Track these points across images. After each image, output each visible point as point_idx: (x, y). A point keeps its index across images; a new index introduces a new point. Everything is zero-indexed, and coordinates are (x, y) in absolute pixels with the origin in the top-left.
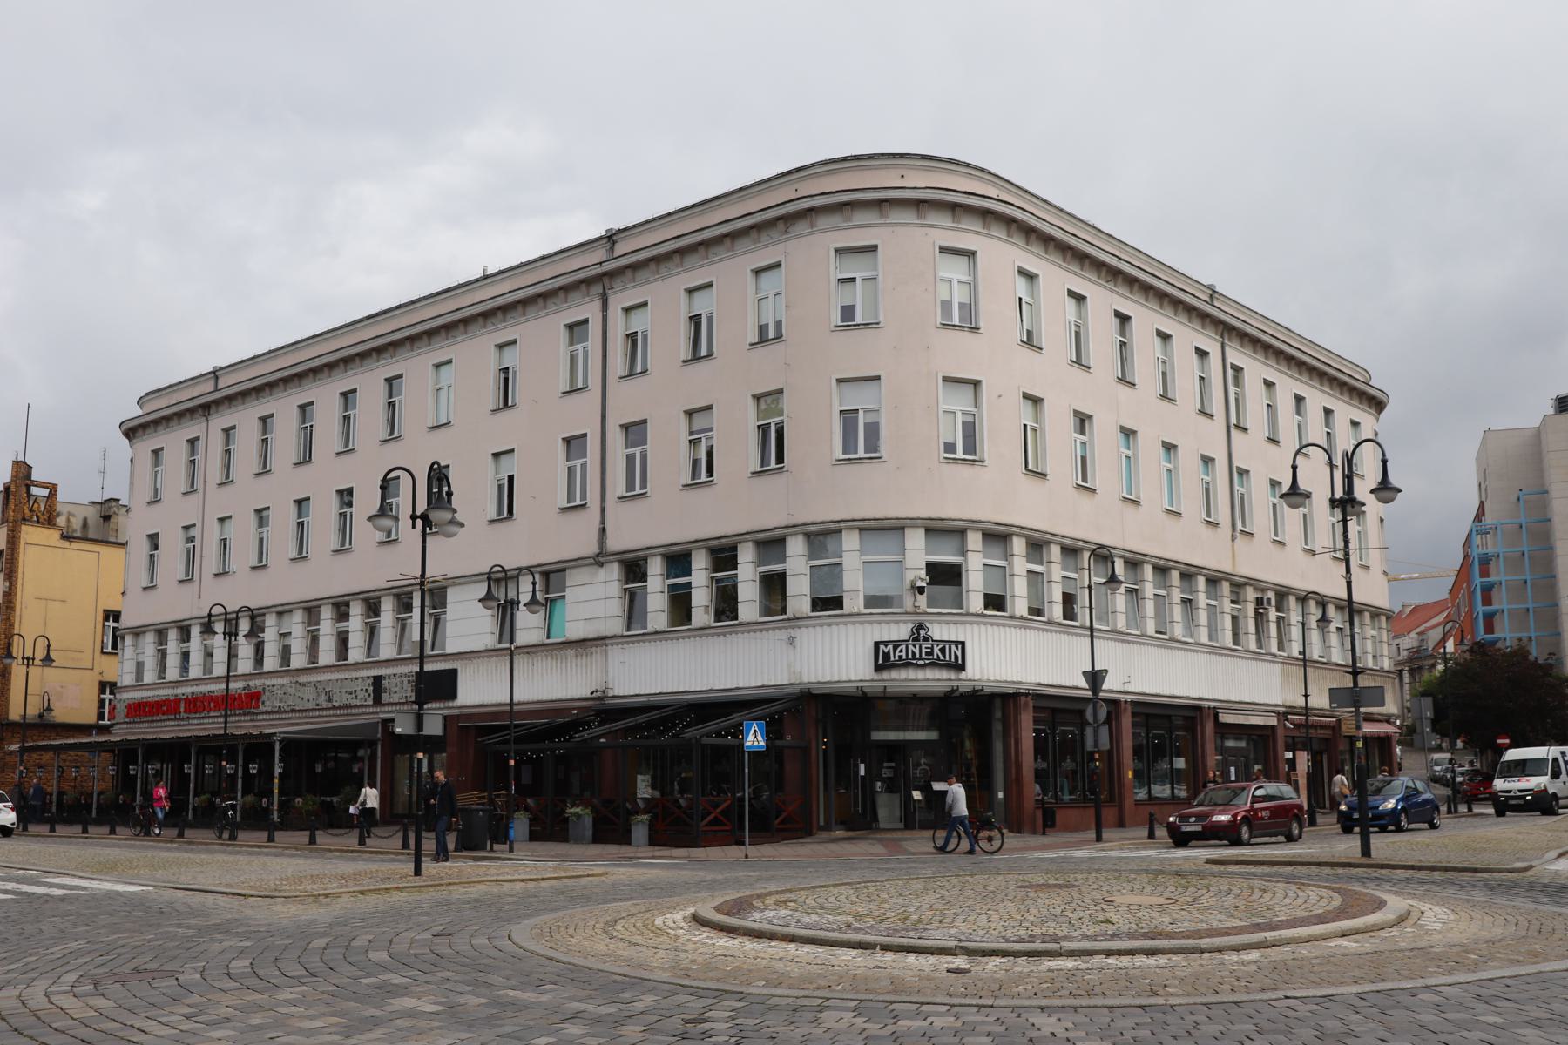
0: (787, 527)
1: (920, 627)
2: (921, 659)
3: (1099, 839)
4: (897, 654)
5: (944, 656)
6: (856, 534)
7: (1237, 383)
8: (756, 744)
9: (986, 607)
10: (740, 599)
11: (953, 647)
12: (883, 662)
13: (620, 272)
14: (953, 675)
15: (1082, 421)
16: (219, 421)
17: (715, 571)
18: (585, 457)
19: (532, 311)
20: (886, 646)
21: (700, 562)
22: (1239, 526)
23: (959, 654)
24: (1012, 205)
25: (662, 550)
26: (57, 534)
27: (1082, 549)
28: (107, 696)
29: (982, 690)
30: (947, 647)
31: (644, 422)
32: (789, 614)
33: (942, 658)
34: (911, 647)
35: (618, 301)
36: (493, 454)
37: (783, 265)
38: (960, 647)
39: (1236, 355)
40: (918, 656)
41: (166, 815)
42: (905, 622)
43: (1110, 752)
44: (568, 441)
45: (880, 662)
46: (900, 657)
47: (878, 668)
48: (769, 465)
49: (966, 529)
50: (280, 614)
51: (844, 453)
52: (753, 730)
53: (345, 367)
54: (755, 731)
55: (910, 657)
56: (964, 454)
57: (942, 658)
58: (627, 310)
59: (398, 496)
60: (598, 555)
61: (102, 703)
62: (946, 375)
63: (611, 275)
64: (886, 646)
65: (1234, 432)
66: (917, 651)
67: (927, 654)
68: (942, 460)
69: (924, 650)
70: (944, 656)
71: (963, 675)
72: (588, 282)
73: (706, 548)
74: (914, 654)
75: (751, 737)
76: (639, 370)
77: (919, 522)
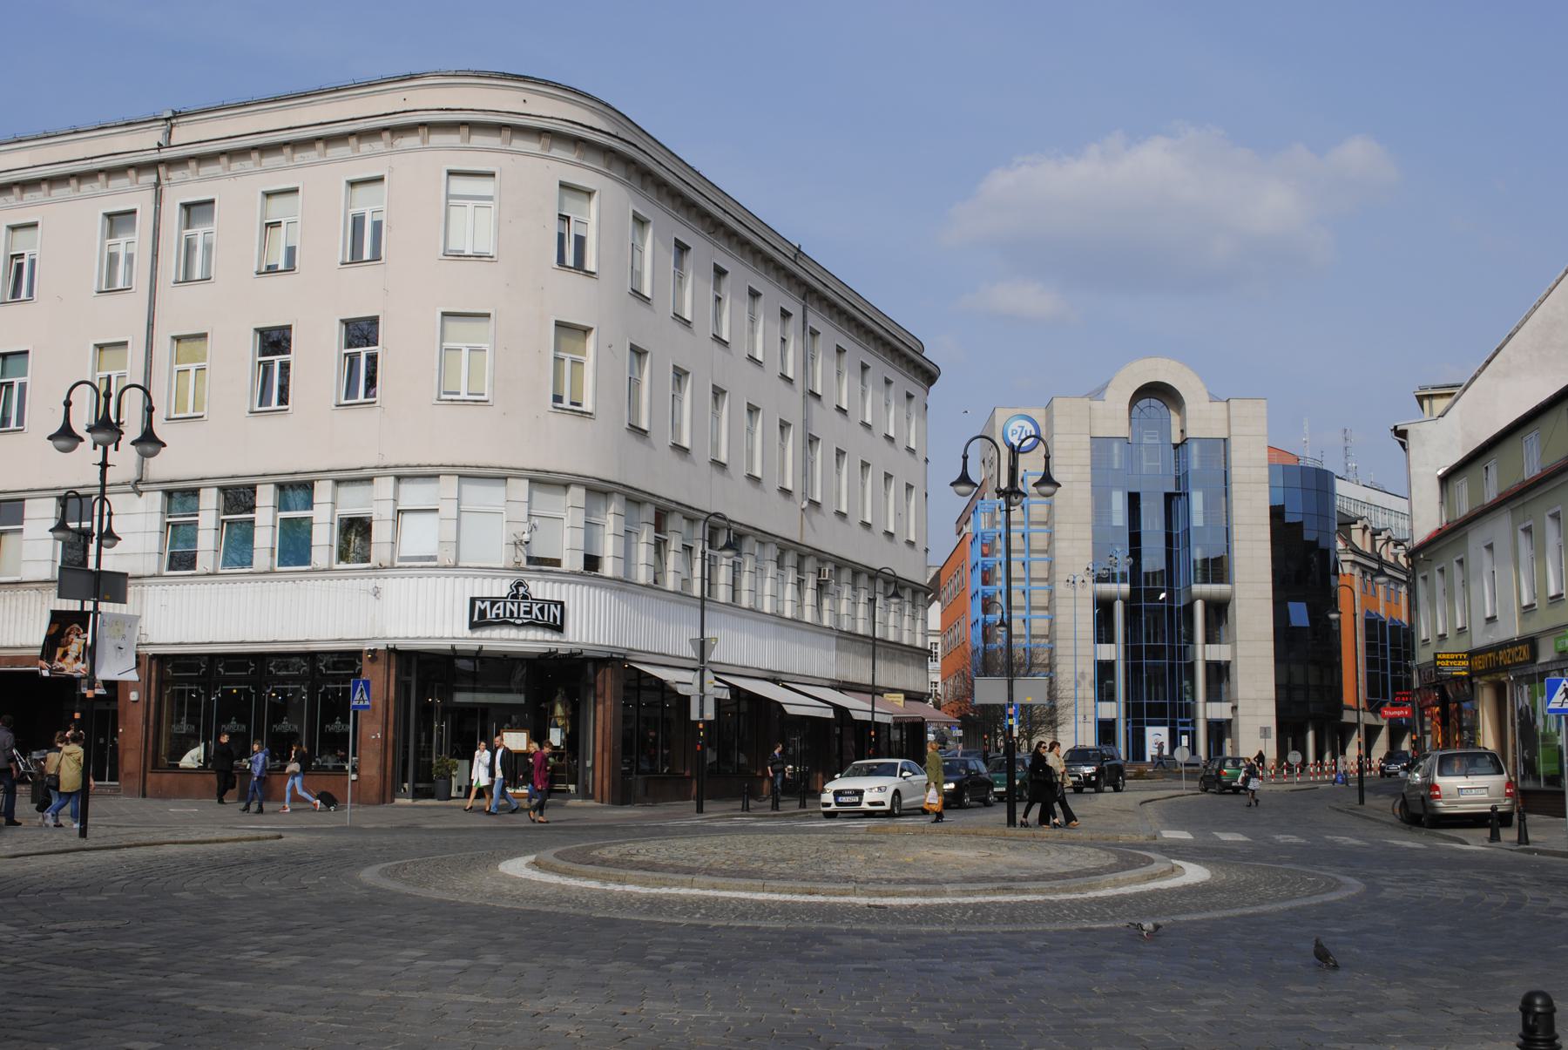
0: (376, 468)
1: (519, 584)
2: (518, 618)
3: (700, 810)
4: (495, 611)
5: (543, 616)
8: (361, 703)
10: (314, 543)
11: (552, 607)
12: (479, 621)
13: (181, 162)
17: (226, 513)
18: (25, 375)
19: (59, 192)
20: (483, 602)
21: (210, 500)
23: (558, 615)
24: (635, 146)
27: (700, 519)
29: (582, 653)
30: (546, 606)
32: (374, 562)
33: (540, 618)
34: (509, 605)
36: (174, 338)
37: (39, 226)
38: (559, 606)
40: (516, 615)
42: (503, 578)
44: (263, 333)
45: (476, 619)
46: (497, 615)
47: (473, 626)
48: (356, 397)
50: (399, 478)
51: (17, 426)
54: (362, 689)
55: (508, 615)
57: (540, 618)
59: (289, 353)
60: (139, 481)
63: (172, 163)
64: (483, 602)
66: (515, 610)
67: (526, 612)
69: (522, 609)
70: (543, 616)
72: (140, 168)
73: (163, 491)
74: (512, 612)
75: (358, 696)
76: (197, 275)
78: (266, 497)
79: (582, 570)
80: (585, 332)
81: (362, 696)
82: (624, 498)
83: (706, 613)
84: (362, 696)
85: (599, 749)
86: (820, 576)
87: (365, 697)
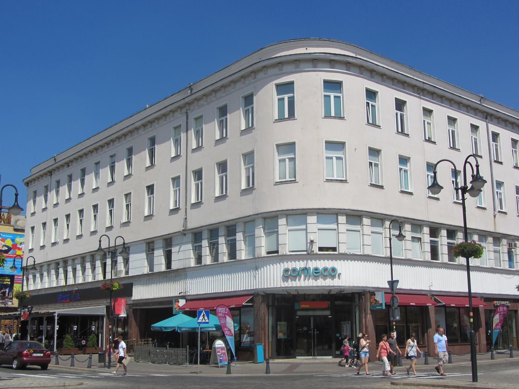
7: (494, 140)
8: (204, 321)
9: (319, 251)
15: (404, 160)
22: (498, 209)
25: (207, 227)
29: (344, 291)
31: (442, 188)
35: (193, 115)
39: (493, 128)
41: (50, 350)
43: (204, 308)
49: (362, 216)
52: (202, 314)
53: (96, 152)
54: (204, 315)
56: (337, 177)
58: (196, 119)
62: (327, 140)
63: (189, 104)
65: (494, 165)
68: (325, 181)
72: (180, 108)
77: (314, 211)
78: (205, 234)
79: (430, 260)
80: (343, 144)
81: (204, 318)
82: (370, 217)
83: (471, 273)
84: (204, 318)
85: (134, 334)
86: (509, 247)
87: (206, 318)
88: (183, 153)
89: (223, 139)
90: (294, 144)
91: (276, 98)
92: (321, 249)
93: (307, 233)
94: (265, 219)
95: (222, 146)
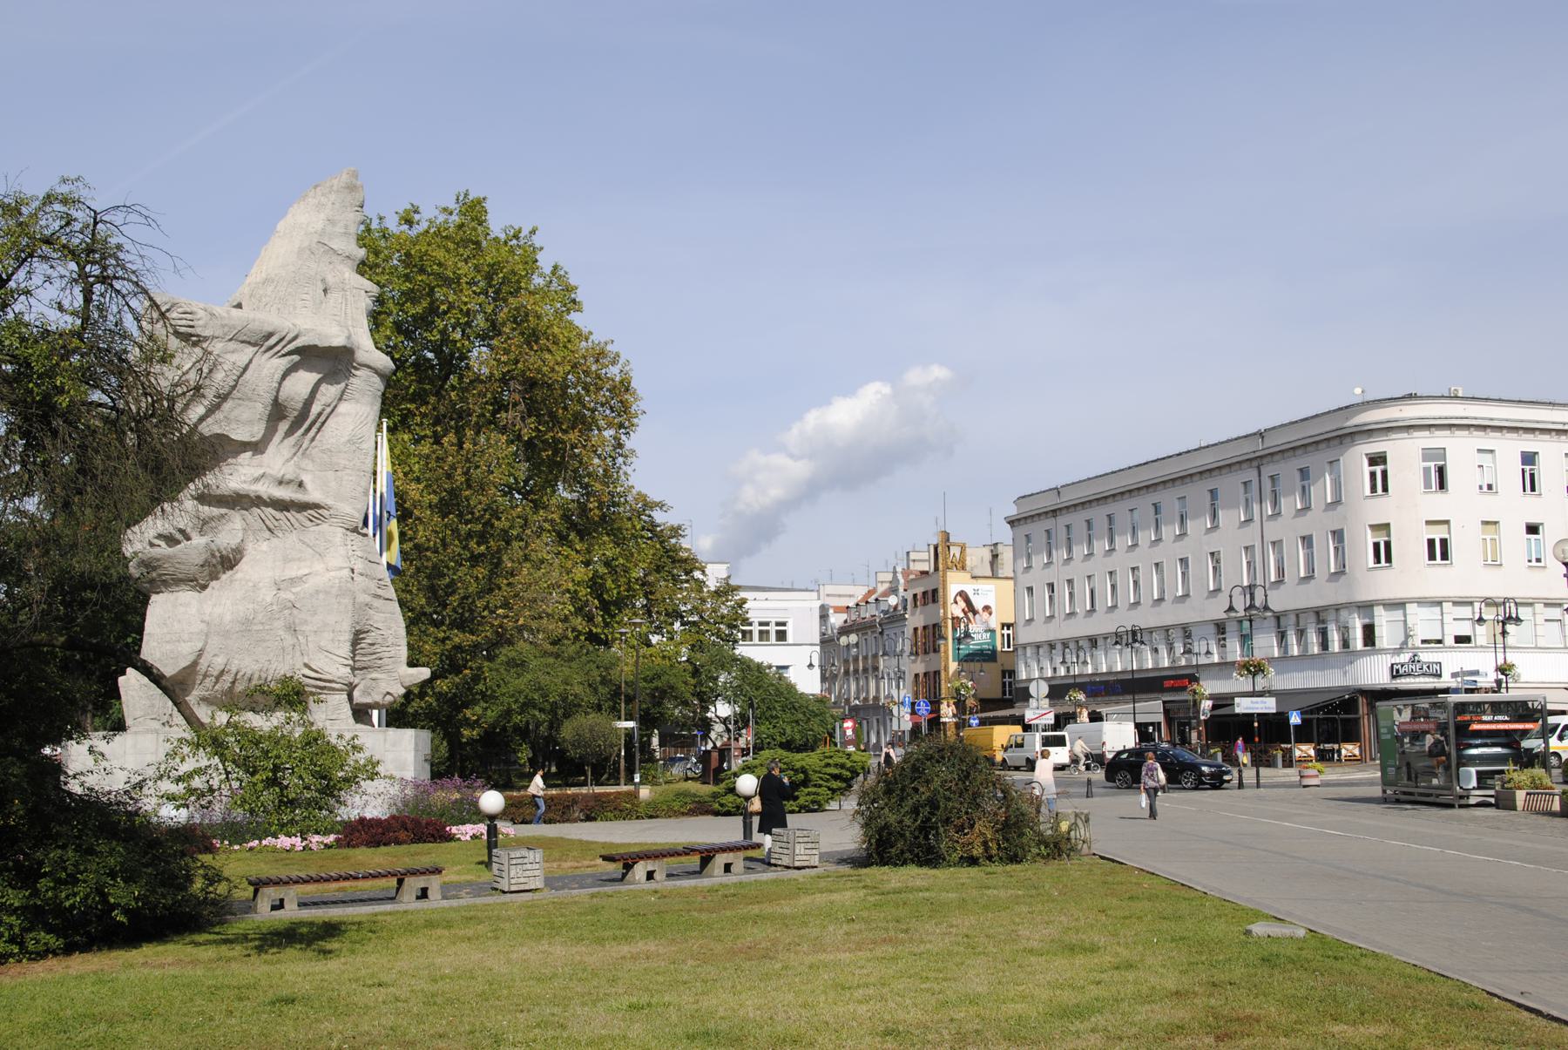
1: (1415, 656)
6: (1381, 607)
9: (1456, 642)
12: (1395, 674)
14: (1436, 680)
16: (1063, 520)
26: (969, 576)
28: (1007, 680)
47: (1394, 677)
61: (1004, 684)
71: (1442, 680)
88: (1257, 517)
89: (1049, 563)
90: (1388, 525)
91: (1367, 469)
92: (1424, 642)
93: (1442, 624)
94: (1359, 607)
95: (1215, 535)
